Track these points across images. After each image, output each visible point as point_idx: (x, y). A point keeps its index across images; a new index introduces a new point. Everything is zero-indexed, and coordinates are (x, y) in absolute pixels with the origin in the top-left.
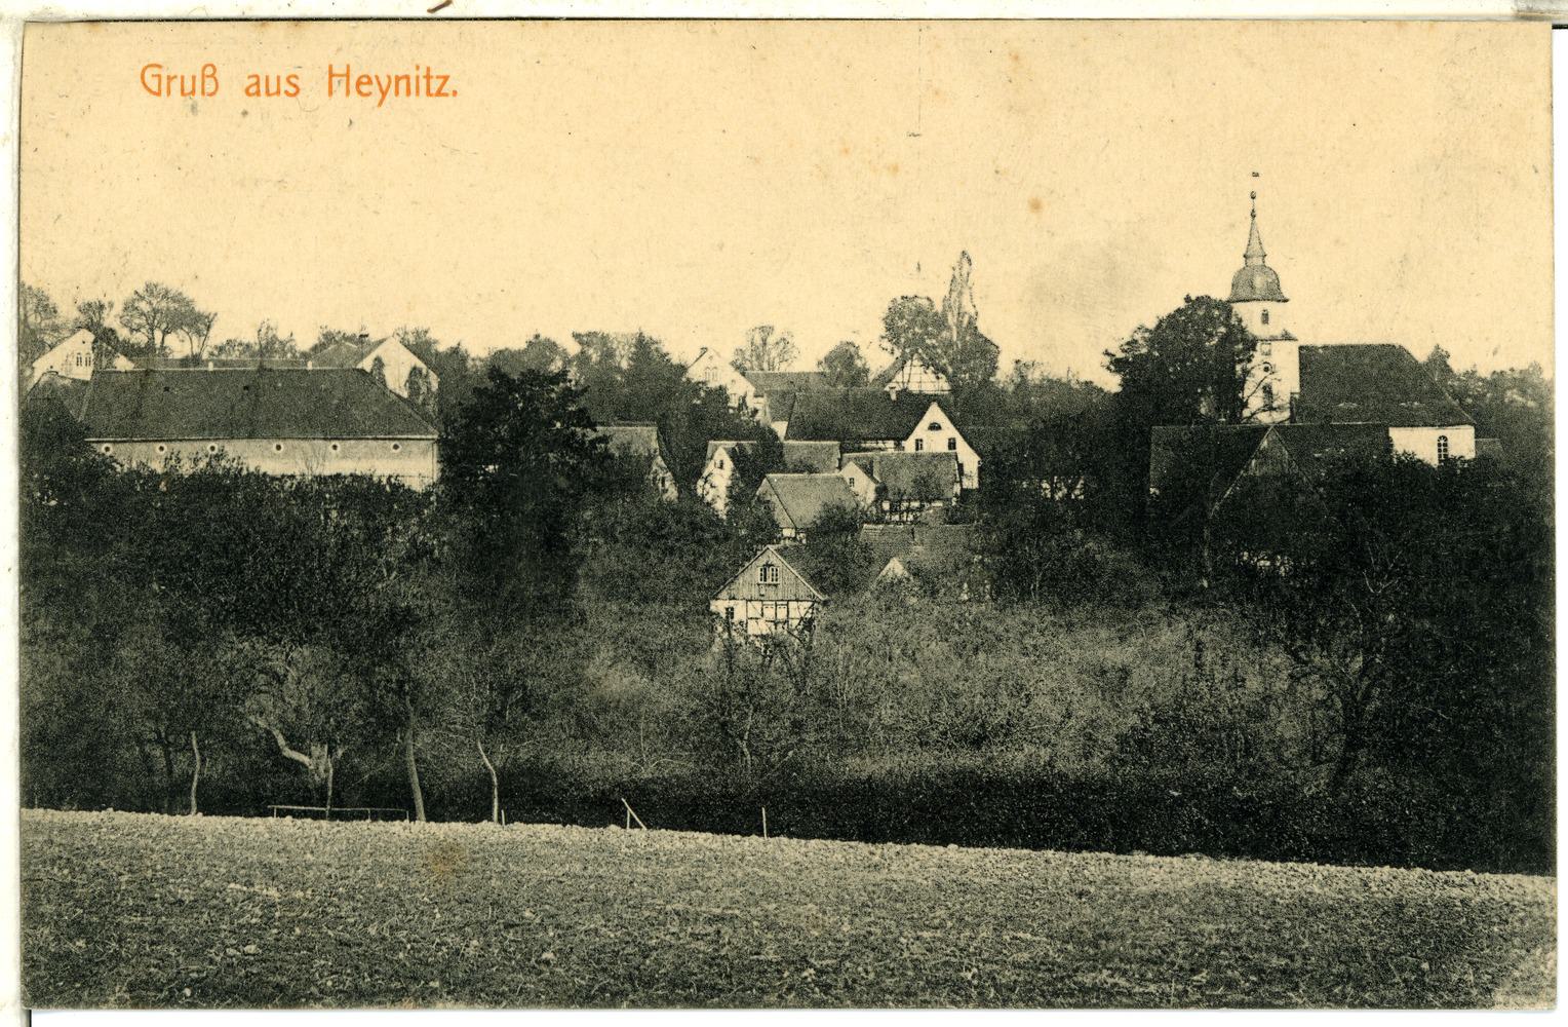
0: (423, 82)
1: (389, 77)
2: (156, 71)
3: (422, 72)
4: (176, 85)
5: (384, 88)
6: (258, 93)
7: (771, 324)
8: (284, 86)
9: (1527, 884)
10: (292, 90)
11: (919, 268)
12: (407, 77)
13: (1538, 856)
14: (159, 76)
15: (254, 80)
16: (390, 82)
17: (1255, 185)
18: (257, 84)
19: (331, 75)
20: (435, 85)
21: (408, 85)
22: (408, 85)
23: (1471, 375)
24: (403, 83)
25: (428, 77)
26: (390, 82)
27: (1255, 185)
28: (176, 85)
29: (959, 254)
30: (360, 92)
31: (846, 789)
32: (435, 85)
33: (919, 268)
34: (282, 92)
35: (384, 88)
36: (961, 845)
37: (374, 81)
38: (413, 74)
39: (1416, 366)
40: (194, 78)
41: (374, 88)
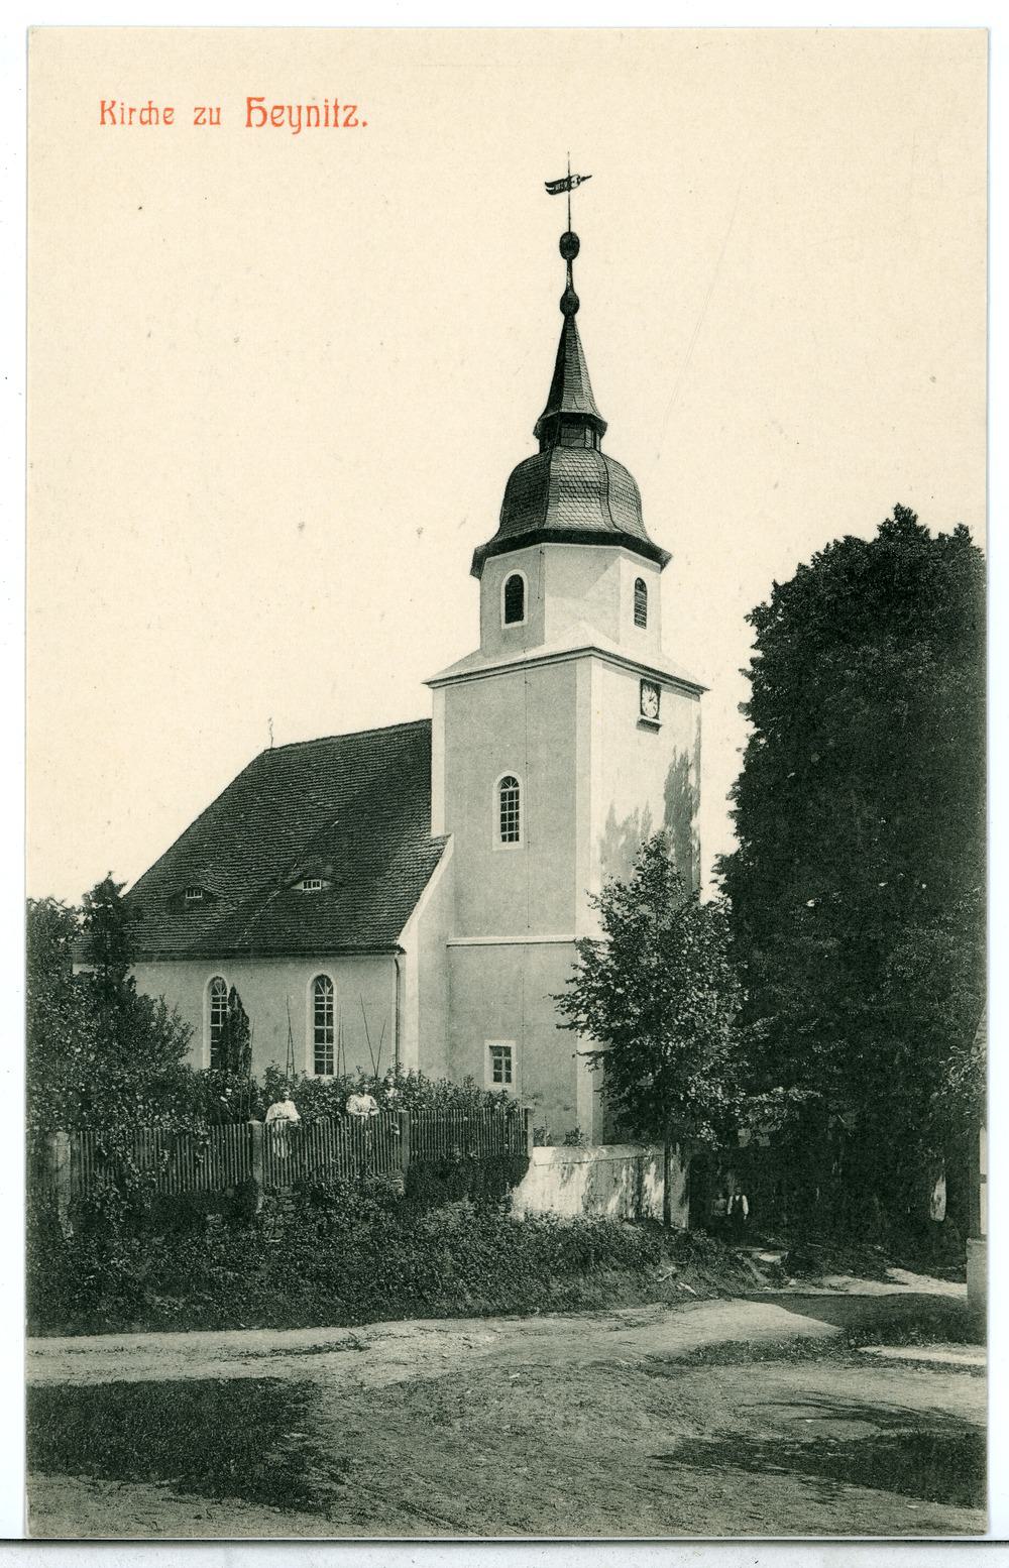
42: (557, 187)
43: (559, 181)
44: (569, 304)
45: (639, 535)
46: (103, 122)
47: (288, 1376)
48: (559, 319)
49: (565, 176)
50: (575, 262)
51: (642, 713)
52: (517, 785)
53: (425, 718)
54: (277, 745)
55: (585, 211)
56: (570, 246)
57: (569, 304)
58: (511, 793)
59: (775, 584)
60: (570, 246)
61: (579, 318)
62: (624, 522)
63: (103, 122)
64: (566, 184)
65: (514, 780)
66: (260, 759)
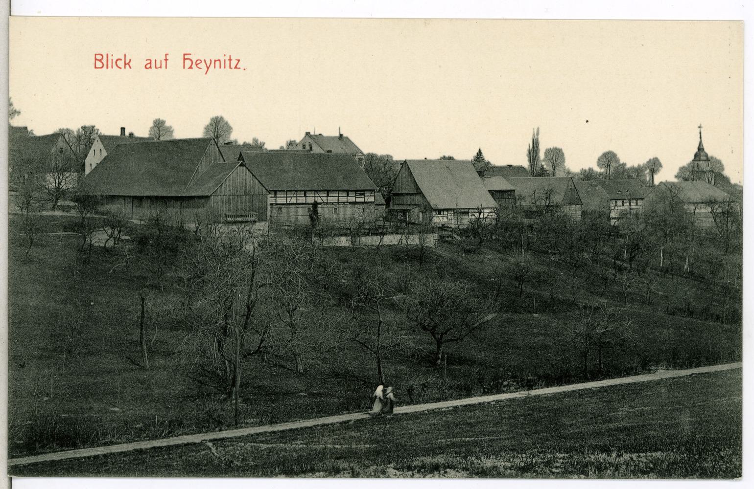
0: (227, 62)
1: (211, 60)
5: (208, 66)
6: (151, 67)
7: (650, 156)
15: (149, 62)
17: (138, 63)
18: (150, 63)
20: (234, 63)
23: (644, 164)
24: (217, 63)
25: (230, 60)
27: (138, 63)
30: (102, 55)
31: (103, 136)
32: (234, 63)
35: (208, 66)
36: (258, 146)
37: (203, 62)
39: (148, 139)
41: (203, 65)
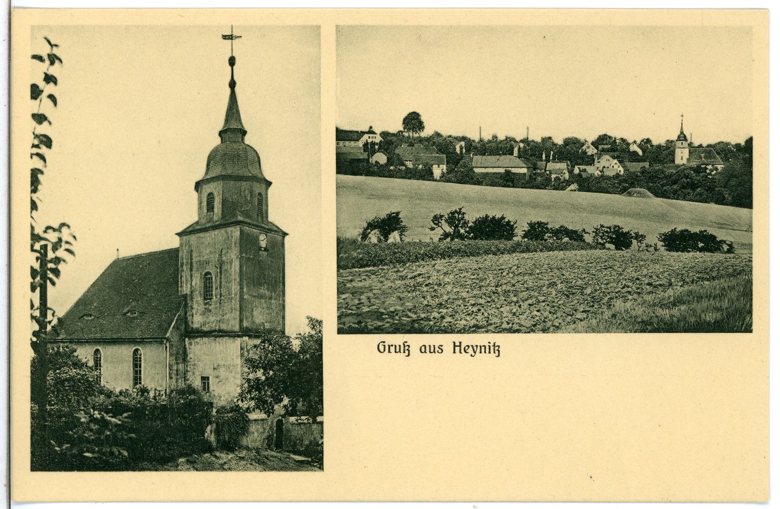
0: (492, 348)
2: (383, 344)
3: (492, 344)
4: (392, 349)
8: (437, 349)
9: (743, 211)
10: (440, 351)
11: (682, 159)
12: (485, 346)
13: (749, 205)
14: (384, 346)
16: (385, 348)
19: (455, 346)
21: (430, 349)
22: (430, 349)
26: (385, 348)
28: (392, 349)
29: (633, 141)
33: (682, 159)
34: (436, 351)
38: (487, 345)
40: (400, 346)
42: (227, 37)
43: (228, 36)
44: (232, 84)
45: (259, 176)
46: (454, 352)
47: (219, 173)
48: (228, 91)
49: (231, 34)
50: (234, 67)
51: (48, 70)
52: (211, 275)
53: (335, 28)
54: (121, 256)
55: (239, 49)
56: (232, 61)
57: (232, 84)
58: (209, 278)
59: (37, 210)
60: (232, 61)
61: (237, 89)
62: (255, 172)
63: (454, 352)
64: (231, 37)
65: (211, 273)
66: (115, 262)
